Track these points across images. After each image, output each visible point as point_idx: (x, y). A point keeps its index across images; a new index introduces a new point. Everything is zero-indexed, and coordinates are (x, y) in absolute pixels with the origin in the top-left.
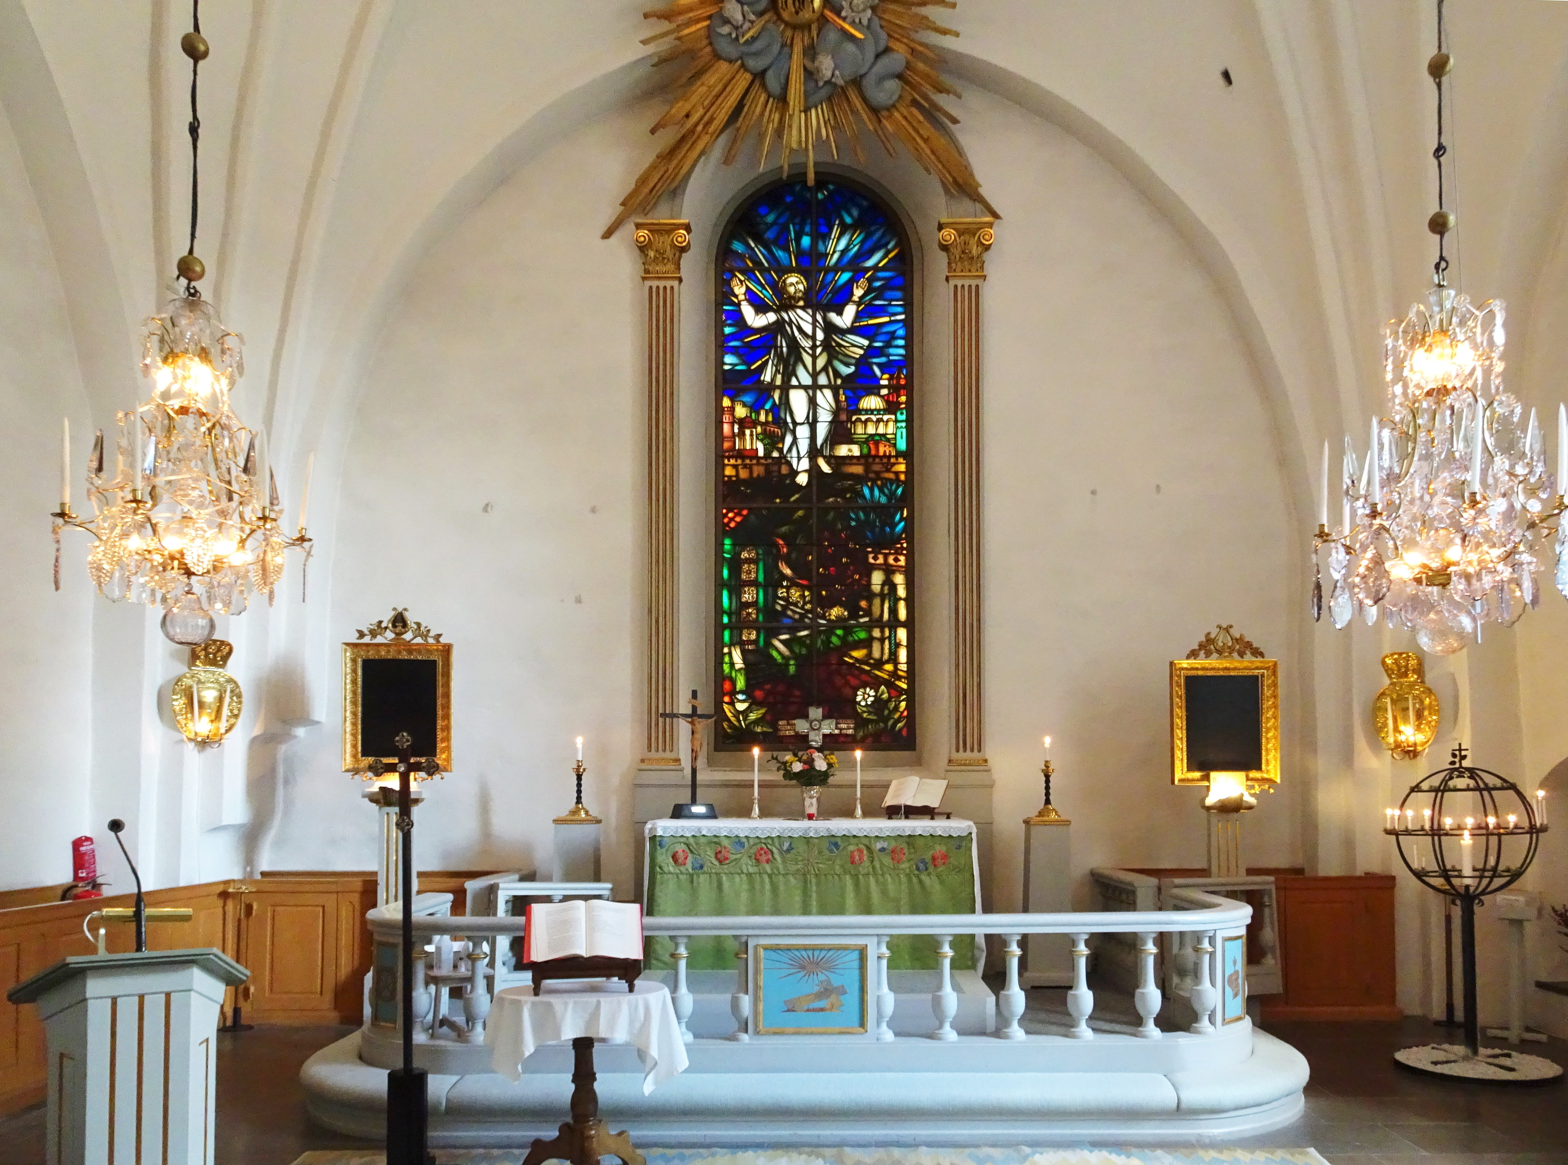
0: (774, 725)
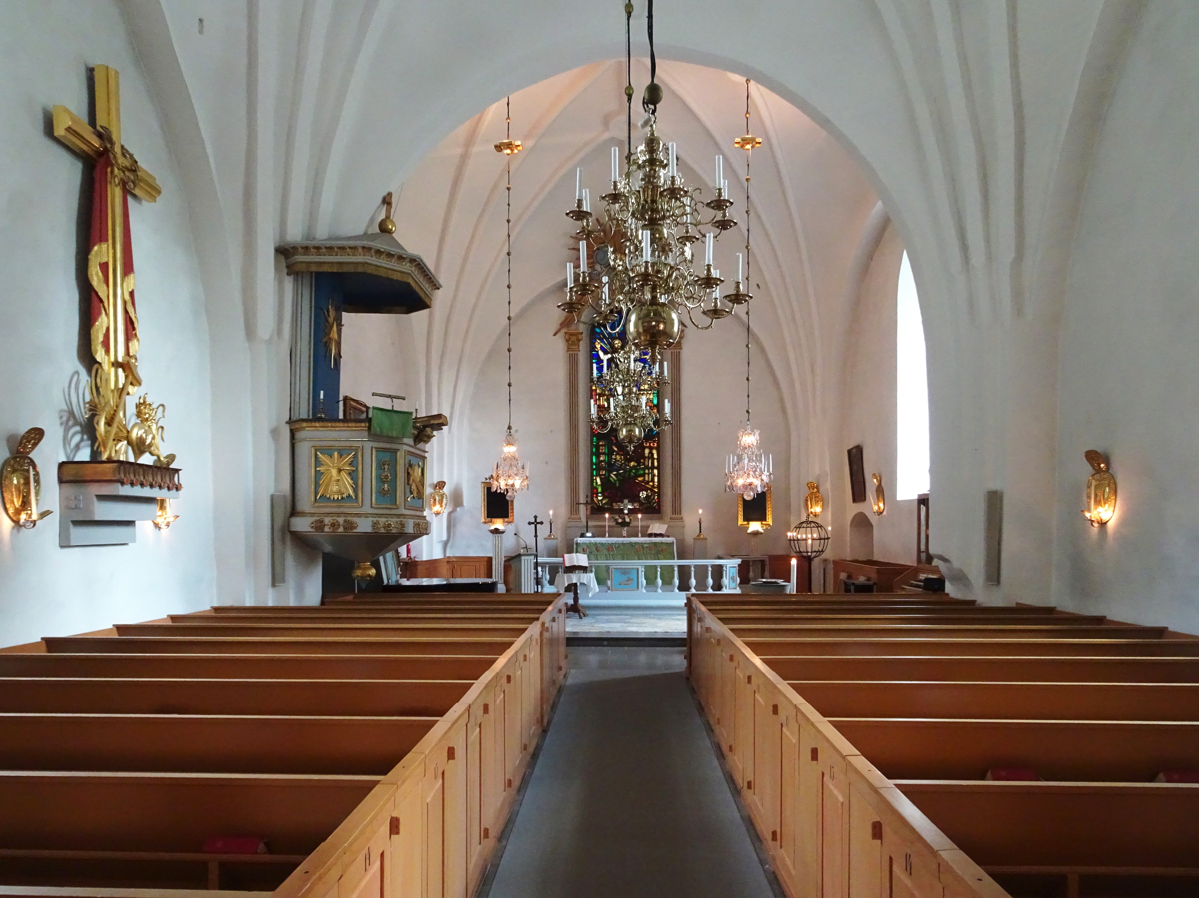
0: (612, 505)
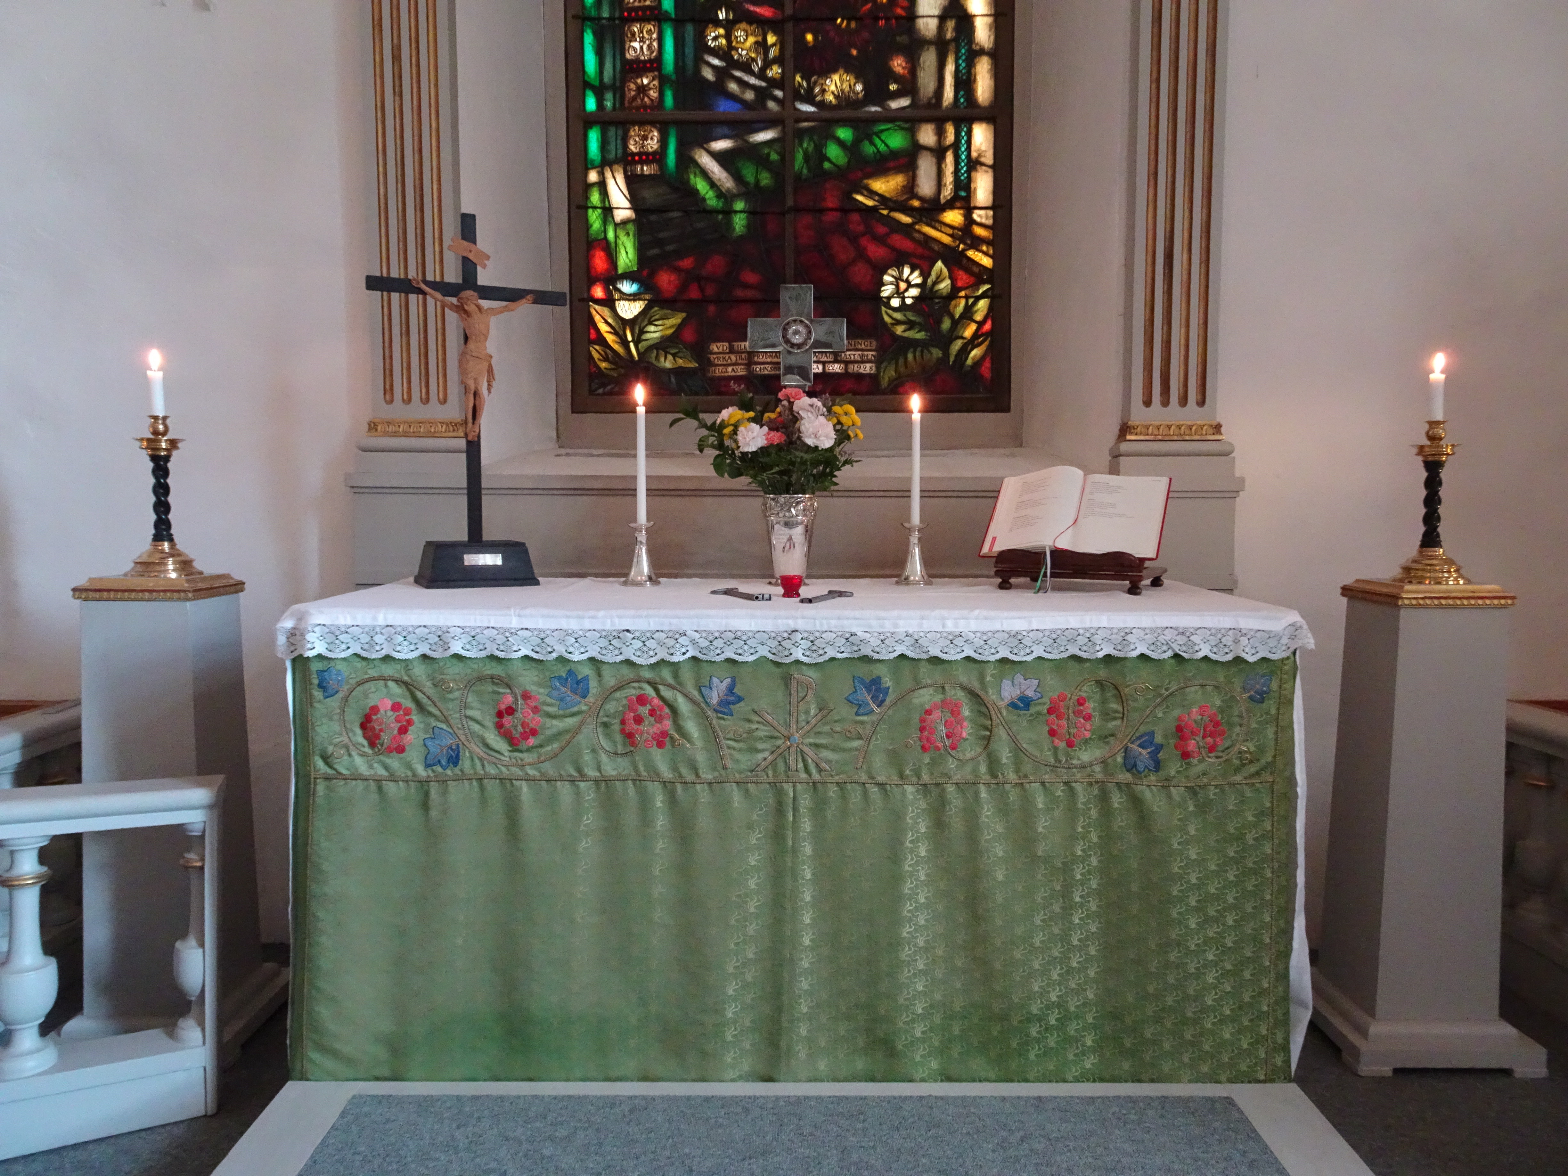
0: (700, 352)
